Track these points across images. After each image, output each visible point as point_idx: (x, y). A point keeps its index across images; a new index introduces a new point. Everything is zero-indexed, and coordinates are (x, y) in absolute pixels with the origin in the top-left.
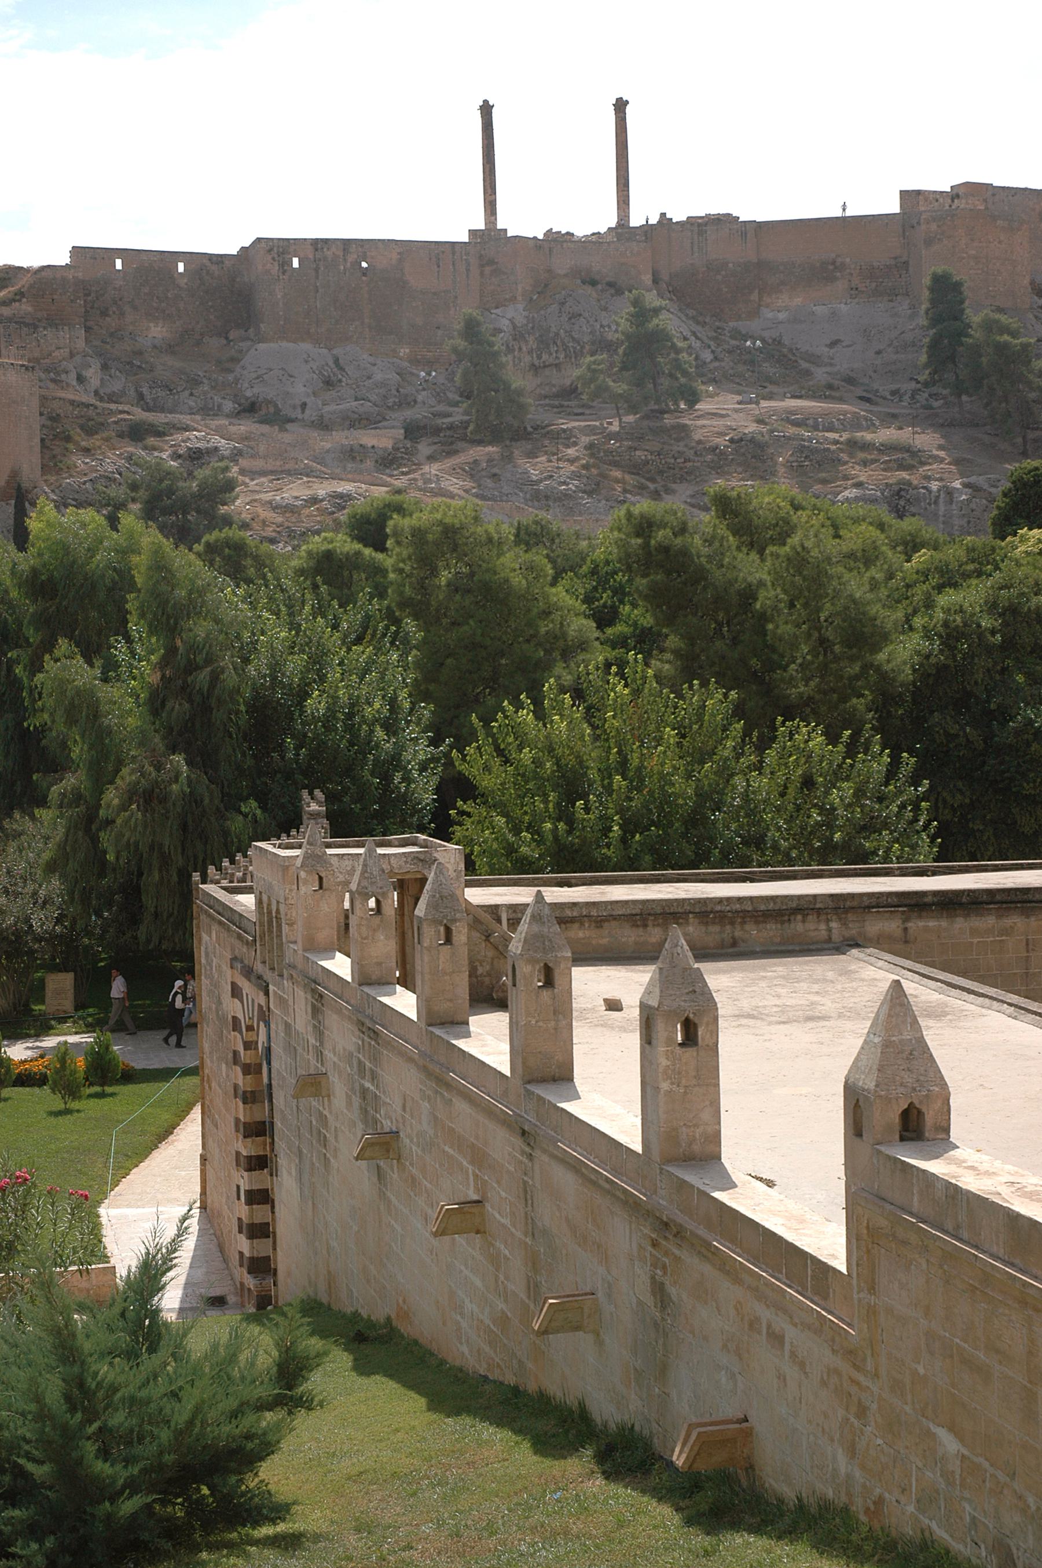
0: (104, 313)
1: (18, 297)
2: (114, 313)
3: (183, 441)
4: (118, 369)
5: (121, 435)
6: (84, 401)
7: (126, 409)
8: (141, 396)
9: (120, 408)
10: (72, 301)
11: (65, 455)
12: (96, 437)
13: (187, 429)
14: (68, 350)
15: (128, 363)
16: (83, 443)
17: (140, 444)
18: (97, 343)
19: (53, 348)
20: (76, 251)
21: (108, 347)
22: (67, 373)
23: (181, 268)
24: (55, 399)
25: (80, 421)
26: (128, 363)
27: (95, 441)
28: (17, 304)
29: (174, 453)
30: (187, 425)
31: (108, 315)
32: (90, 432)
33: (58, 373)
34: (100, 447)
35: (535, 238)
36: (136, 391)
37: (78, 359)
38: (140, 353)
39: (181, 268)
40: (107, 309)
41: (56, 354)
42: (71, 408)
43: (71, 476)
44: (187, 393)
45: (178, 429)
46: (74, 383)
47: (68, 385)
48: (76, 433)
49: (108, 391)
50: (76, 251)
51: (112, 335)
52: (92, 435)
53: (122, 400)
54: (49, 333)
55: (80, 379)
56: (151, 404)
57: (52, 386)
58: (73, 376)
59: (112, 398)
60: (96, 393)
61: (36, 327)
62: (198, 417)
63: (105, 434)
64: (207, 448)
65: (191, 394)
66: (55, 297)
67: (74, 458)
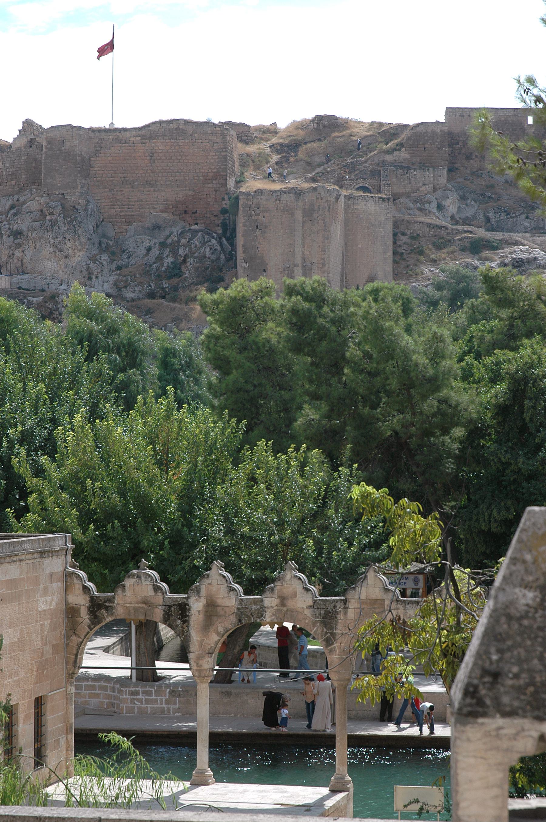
0: (469, 157)
1: (398, 147)
2: (476, 156)
3: (510, 253)
4: (473, 199)
5: (463, 250)
6: (438, 223)
7: (470, 229)
8: (488, 220)
9: (465, 229)
10: (439, 149)
11: (416, 265)
12: (443, 251)
13: (516, 243)
14: (431, 186)
15: (482, 195)
16: (433, 256)
17: (477, 256)
18: (461, 180)
19: (421, 184)
20: (450, 111)
21: (468, 182)
22: (430, 203)
23: (530, 120)
24: (416, 222)
25: (434, 239)
26: (482, 195)
27: (442, 254)
28: (398, 152)
29: (501, 263)
30: (517, 241)
31: (471, 159)
32: (439, 248)
33: (423, 204)
34: (444, 259)
35: (438, 122)
36: (485, 216)
37: (439, 193)
38: (492, 187)
39: (530, 120)
40: (471, 154)
41: (423, 189)
42: (428, 230)
43: (418, 281)
44: (523, 216)
45: (510, 244)
46: (435, 210)
47: (430, 212)
48: (429, 249)
49: (463, 216)
50: (450, 111)
51: (473, 173)
52: (441, 249)
53: (473, 223)
54: (418, 174)
55: (440, 207)
56: (495, 225)
57: (418, 213)
58: (434, 205)
59: (466, 222)
60: (452, 217)
61: (408, 168)
62: (528, 235)
63: (451, 249)
64: (528, 259)
65: (527, 217)
66: (426, 146)
67: (423, 267)
